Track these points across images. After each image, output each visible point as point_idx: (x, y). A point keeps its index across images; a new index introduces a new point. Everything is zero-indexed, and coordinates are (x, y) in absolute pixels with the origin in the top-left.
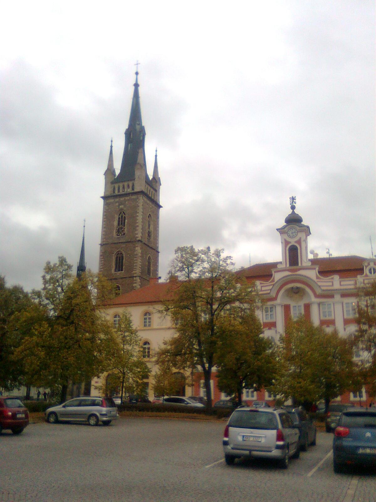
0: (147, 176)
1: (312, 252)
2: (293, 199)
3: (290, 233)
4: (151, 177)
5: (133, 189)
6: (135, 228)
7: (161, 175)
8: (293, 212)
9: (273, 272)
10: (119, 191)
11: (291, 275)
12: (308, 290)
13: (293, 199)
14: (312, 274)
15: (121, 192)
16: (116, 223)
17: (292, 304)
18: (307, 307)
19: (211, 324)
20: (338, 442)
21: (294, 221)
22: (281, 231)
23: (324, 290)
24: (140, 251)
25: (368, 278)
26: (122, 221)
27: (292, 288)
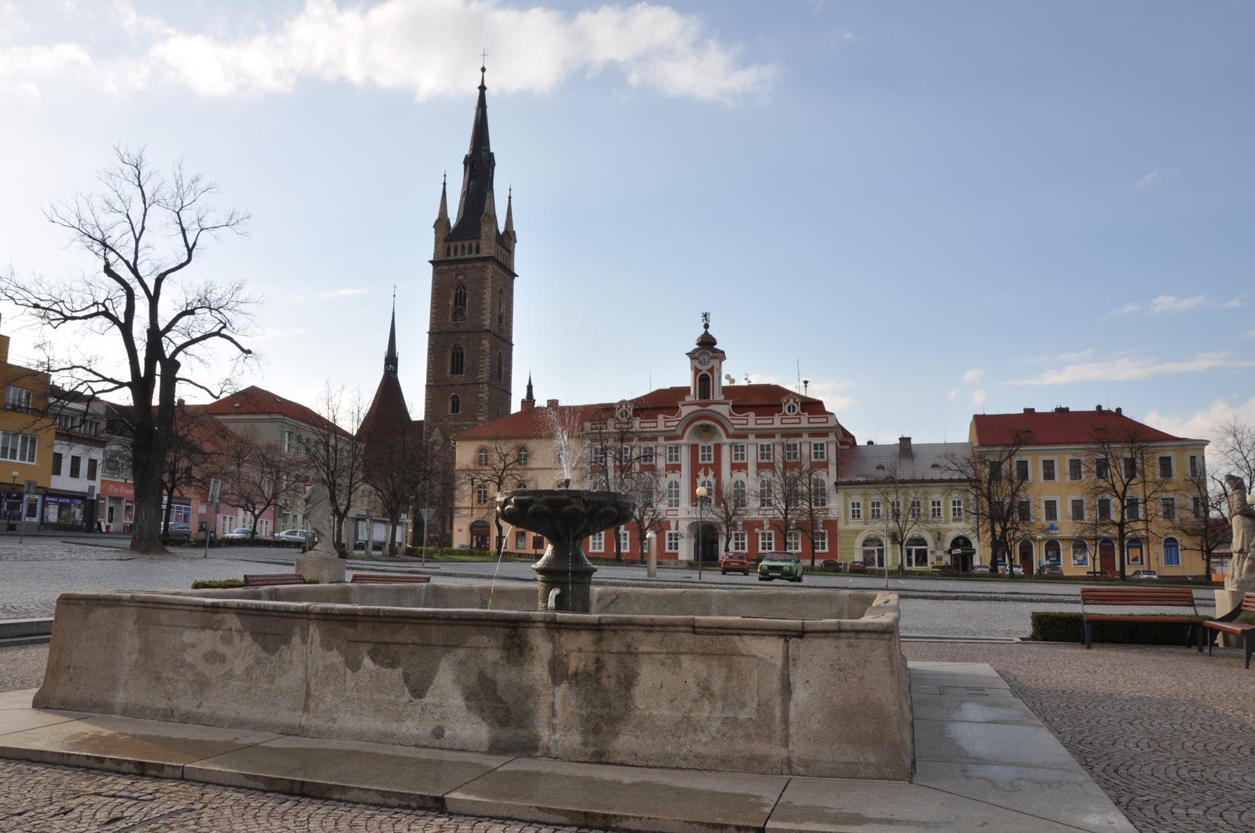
0: (497, 231)
1: (728, 377)
4: (501, 230)
5: (478, 252)
6: (480, 312)
7: (516, 227)
8: (706, 332)
10: (456, 254)
14: (725, 410)
15: (459, 256)
16: (451, 302)
17: (701, 444)
18: (718, 448)
21: (707, 343)
22: (692, 355)
26: (460, 299)
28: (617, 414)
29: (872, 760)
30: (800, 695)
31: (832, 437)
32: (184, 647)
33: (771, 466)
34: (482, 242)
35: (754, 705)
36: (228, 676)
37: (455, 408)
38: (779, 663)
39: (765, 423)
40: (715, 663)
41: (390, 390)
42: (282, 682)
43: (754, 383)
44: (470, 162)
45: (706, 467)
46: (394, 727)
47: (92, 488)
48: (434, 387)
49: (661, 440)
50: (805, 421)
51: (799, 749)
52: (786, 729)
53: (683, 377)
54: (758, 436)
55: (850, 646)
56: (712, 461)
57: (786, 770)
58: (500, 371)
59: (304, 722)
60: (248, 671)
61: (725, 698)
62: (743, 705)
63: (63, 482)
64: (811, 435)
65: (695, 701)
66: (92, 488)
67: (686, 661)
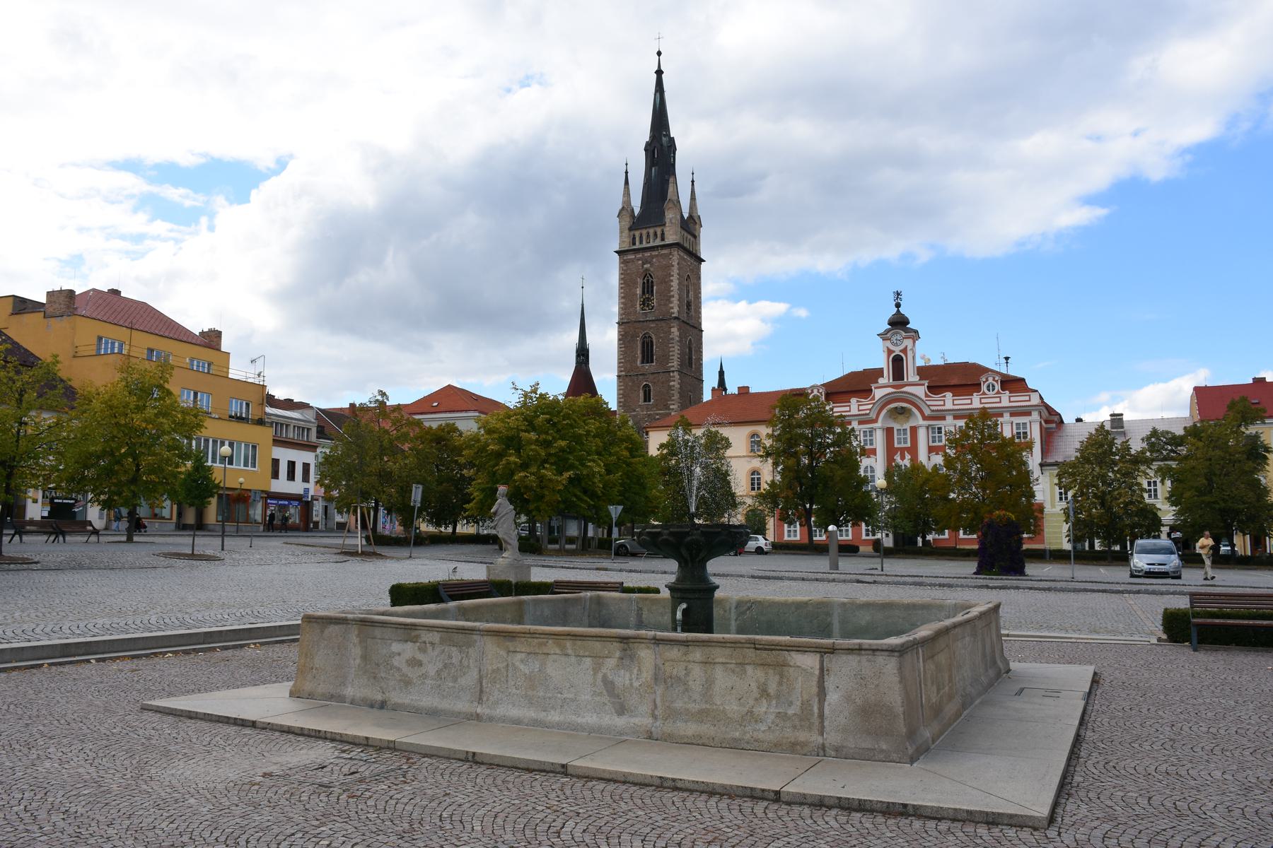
0: (682, 216)
3: (894, 339)
4: (686, 215)
5: (663, 239)
6: (669, 299)
7: (701, 211)
10: (641, 242)
12: (914, 410)
13: (898, 294)
14: (920, 391)
15: (645, 245)
16: (639, 291)
17: (896, 426)
18: (914, 430)
19: (810, 467)
20: (60, 390)
21: (899, 322)
22: (884, 336)
24: (677, 333)
26: (648, 288)
29: (884, 747)
30: (833, 697)
31: (1035, 415)
32: (392, 655)
34: (667, 229)
35: (799, 703)
36: (425, 676)
37: (647, 398)
38: (817, 672)
40: (771, 672)
41: (582, 381)
42: (463, 681)
44: (650, 149)
45: (902, 450)
46: (542, 715)
47: (307, 490)
48: (626, 377)
50: (1006, 400)
51: (832, 738)
52: (822, 722)
53: (876, 358)
54: (1012, 415)
55: (869, 661)
56: (909, 445)
57: (821, 753)
58: (690, 358)
59: (479, 710)
60: (438, 673)
61: (778, 697)
62: (790, 704)
63: (281, 485)
65: (756, 699)
66: (307, 490)
67: (749, 669)
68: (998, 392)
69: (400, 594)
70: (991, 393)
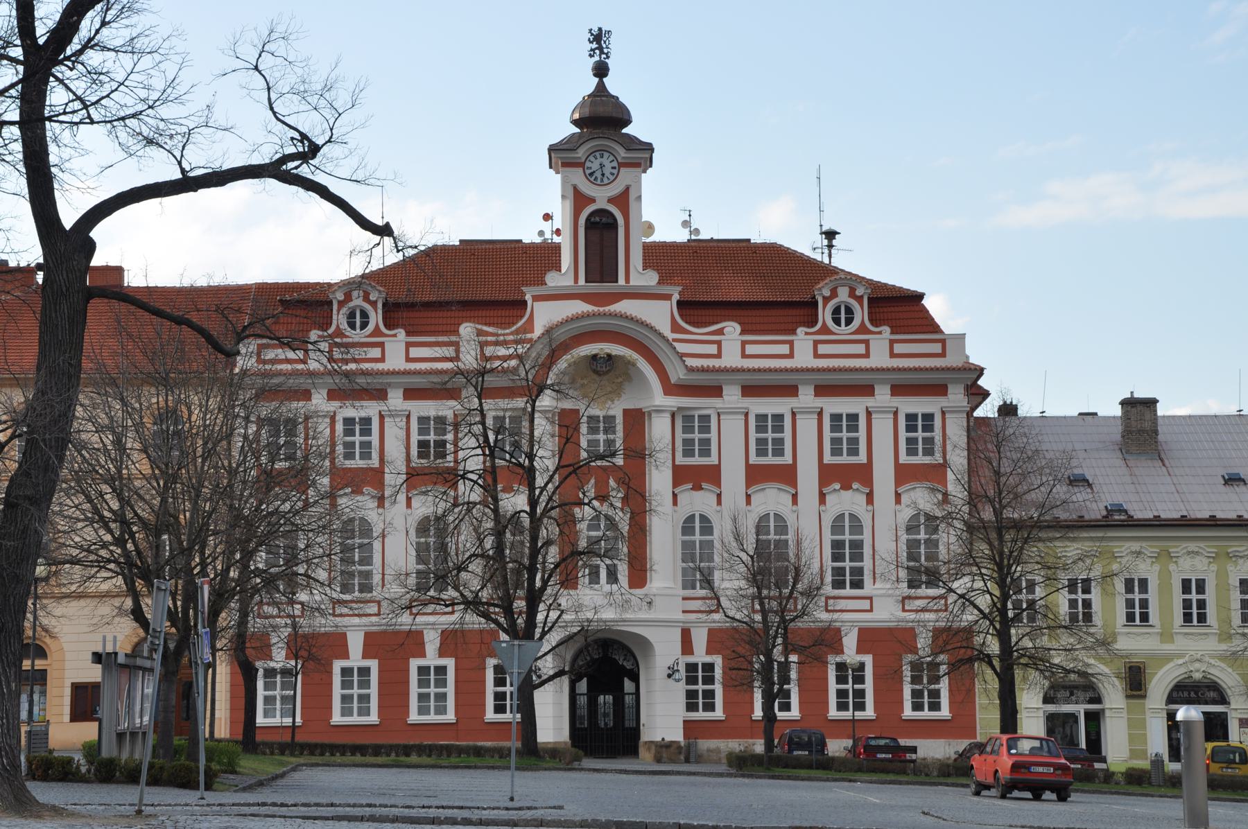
2: (598, 38)
8: (601, 89)
9: (528, 298)
11: (588, 316)
13: (598, 38)
14: (659, 314)
18: (636, 420)
21: (602, 120)
22: (561, 155)
23: (691, 370)
25: (345, 340)
27: (594, 357)
28: (339, 319)
33: (787, 475)
39: (768, 352)
43: (704, 236)
49: (395, 399)
50: (881, 351)
53: (530, 207)
54: (749, 391)
64: (897, 390)
68: (862, 329)
69: (561, 808)
70: (843, 331)
